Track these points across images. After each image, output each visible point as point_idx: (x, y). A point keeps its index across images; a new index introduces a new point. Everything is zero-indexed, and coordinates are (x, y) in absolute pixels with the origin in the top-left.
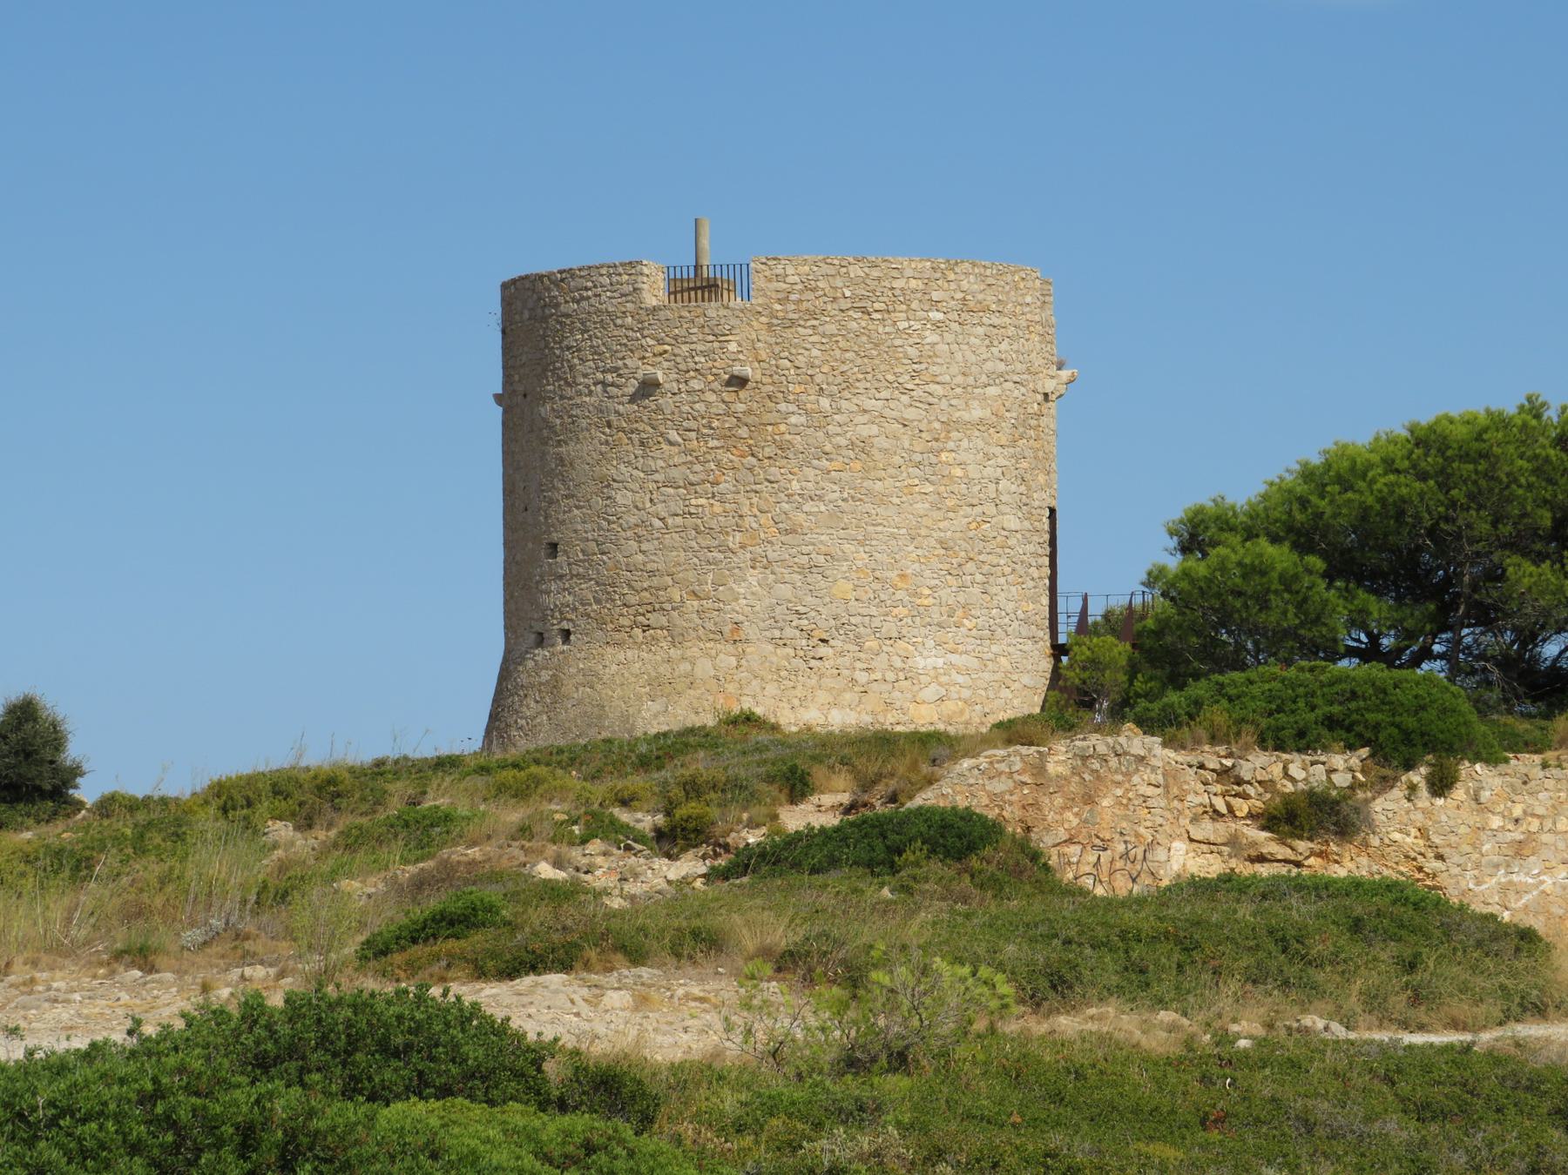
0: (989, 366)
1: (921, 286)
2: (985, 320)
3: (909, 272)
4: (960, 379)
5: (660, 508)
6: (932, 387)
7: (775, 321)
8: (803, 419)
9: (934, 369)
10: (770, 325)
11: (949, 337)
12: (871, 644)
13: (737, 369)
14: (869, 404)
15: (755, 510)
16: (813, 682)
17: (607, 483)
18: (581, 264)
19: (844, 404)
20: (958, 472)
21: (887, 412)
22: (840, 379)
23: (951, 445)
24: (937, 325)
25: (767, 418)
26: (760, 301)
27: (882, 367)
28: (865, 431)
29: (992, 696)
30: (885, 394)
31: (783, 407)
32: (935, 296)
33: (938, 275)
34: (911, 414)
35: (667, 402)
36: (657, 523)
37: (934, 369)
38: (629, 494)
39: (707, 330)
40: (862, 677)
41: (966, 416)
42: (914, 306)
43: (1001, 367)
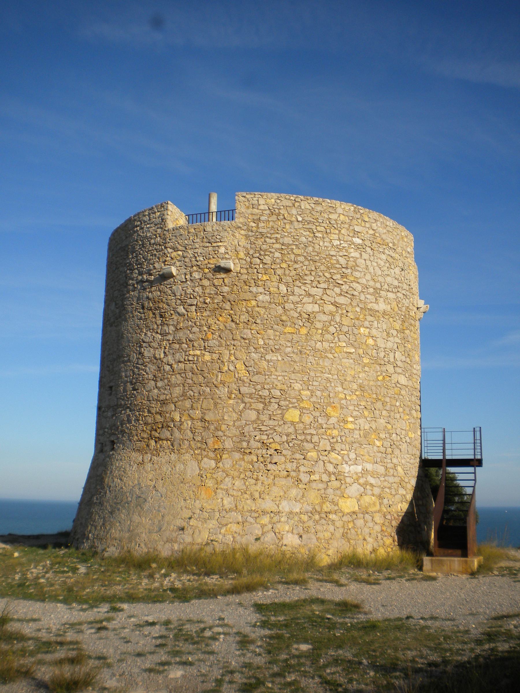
0: (389, 279)
1: (348, 221)
2: (386, 251)
3: (340, 211)
4: (371, 283)
5: (170, 358)
6: (355, 285)
7: (250, 233)
8: (267, 298)
9: (357, 274)
10: (247, 237)
11: (365, 256)
12: (313, 454)
13: (223, 263)
14: (313, 291)
15: (233, 358)
16: (270, 481)
17: (140, 344)
18: (134, 214)
19: (296, 290)
20: (370, 341)
21: (325, 297)
22: (293, 273)
23: (367, 324)
24: (358, 247)
25: (243, 296)
26: (241, 220)
27: (322, 268)
28: (310, 308)
29: (394, 493)
30: (323, 285)
31: (254, 289)
32: (357, 229)
33: (358, 216)
34: (341, 300)
35: (178, 289)
36: (167, 368)
37: (357, 274)
38: (152, 350)
39: (205, 240)
40: (305, 478)
41: (375, 307)
42: (343, 231)
43: (396, 283)
